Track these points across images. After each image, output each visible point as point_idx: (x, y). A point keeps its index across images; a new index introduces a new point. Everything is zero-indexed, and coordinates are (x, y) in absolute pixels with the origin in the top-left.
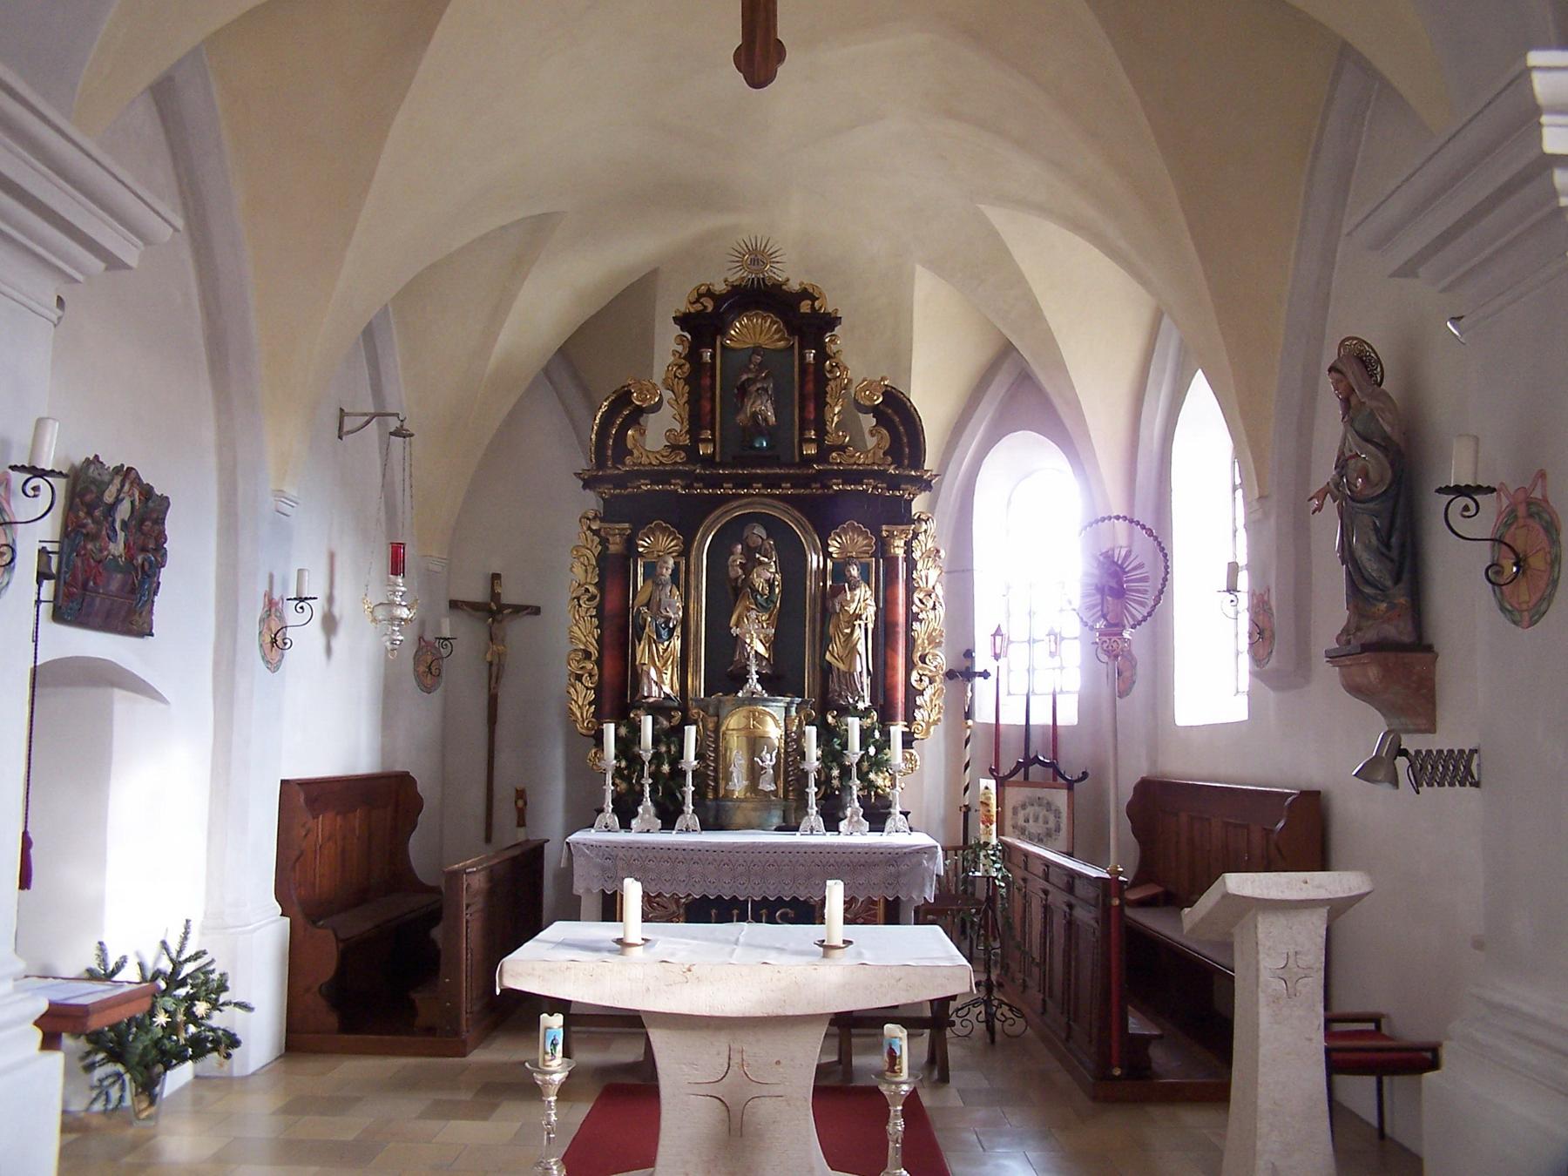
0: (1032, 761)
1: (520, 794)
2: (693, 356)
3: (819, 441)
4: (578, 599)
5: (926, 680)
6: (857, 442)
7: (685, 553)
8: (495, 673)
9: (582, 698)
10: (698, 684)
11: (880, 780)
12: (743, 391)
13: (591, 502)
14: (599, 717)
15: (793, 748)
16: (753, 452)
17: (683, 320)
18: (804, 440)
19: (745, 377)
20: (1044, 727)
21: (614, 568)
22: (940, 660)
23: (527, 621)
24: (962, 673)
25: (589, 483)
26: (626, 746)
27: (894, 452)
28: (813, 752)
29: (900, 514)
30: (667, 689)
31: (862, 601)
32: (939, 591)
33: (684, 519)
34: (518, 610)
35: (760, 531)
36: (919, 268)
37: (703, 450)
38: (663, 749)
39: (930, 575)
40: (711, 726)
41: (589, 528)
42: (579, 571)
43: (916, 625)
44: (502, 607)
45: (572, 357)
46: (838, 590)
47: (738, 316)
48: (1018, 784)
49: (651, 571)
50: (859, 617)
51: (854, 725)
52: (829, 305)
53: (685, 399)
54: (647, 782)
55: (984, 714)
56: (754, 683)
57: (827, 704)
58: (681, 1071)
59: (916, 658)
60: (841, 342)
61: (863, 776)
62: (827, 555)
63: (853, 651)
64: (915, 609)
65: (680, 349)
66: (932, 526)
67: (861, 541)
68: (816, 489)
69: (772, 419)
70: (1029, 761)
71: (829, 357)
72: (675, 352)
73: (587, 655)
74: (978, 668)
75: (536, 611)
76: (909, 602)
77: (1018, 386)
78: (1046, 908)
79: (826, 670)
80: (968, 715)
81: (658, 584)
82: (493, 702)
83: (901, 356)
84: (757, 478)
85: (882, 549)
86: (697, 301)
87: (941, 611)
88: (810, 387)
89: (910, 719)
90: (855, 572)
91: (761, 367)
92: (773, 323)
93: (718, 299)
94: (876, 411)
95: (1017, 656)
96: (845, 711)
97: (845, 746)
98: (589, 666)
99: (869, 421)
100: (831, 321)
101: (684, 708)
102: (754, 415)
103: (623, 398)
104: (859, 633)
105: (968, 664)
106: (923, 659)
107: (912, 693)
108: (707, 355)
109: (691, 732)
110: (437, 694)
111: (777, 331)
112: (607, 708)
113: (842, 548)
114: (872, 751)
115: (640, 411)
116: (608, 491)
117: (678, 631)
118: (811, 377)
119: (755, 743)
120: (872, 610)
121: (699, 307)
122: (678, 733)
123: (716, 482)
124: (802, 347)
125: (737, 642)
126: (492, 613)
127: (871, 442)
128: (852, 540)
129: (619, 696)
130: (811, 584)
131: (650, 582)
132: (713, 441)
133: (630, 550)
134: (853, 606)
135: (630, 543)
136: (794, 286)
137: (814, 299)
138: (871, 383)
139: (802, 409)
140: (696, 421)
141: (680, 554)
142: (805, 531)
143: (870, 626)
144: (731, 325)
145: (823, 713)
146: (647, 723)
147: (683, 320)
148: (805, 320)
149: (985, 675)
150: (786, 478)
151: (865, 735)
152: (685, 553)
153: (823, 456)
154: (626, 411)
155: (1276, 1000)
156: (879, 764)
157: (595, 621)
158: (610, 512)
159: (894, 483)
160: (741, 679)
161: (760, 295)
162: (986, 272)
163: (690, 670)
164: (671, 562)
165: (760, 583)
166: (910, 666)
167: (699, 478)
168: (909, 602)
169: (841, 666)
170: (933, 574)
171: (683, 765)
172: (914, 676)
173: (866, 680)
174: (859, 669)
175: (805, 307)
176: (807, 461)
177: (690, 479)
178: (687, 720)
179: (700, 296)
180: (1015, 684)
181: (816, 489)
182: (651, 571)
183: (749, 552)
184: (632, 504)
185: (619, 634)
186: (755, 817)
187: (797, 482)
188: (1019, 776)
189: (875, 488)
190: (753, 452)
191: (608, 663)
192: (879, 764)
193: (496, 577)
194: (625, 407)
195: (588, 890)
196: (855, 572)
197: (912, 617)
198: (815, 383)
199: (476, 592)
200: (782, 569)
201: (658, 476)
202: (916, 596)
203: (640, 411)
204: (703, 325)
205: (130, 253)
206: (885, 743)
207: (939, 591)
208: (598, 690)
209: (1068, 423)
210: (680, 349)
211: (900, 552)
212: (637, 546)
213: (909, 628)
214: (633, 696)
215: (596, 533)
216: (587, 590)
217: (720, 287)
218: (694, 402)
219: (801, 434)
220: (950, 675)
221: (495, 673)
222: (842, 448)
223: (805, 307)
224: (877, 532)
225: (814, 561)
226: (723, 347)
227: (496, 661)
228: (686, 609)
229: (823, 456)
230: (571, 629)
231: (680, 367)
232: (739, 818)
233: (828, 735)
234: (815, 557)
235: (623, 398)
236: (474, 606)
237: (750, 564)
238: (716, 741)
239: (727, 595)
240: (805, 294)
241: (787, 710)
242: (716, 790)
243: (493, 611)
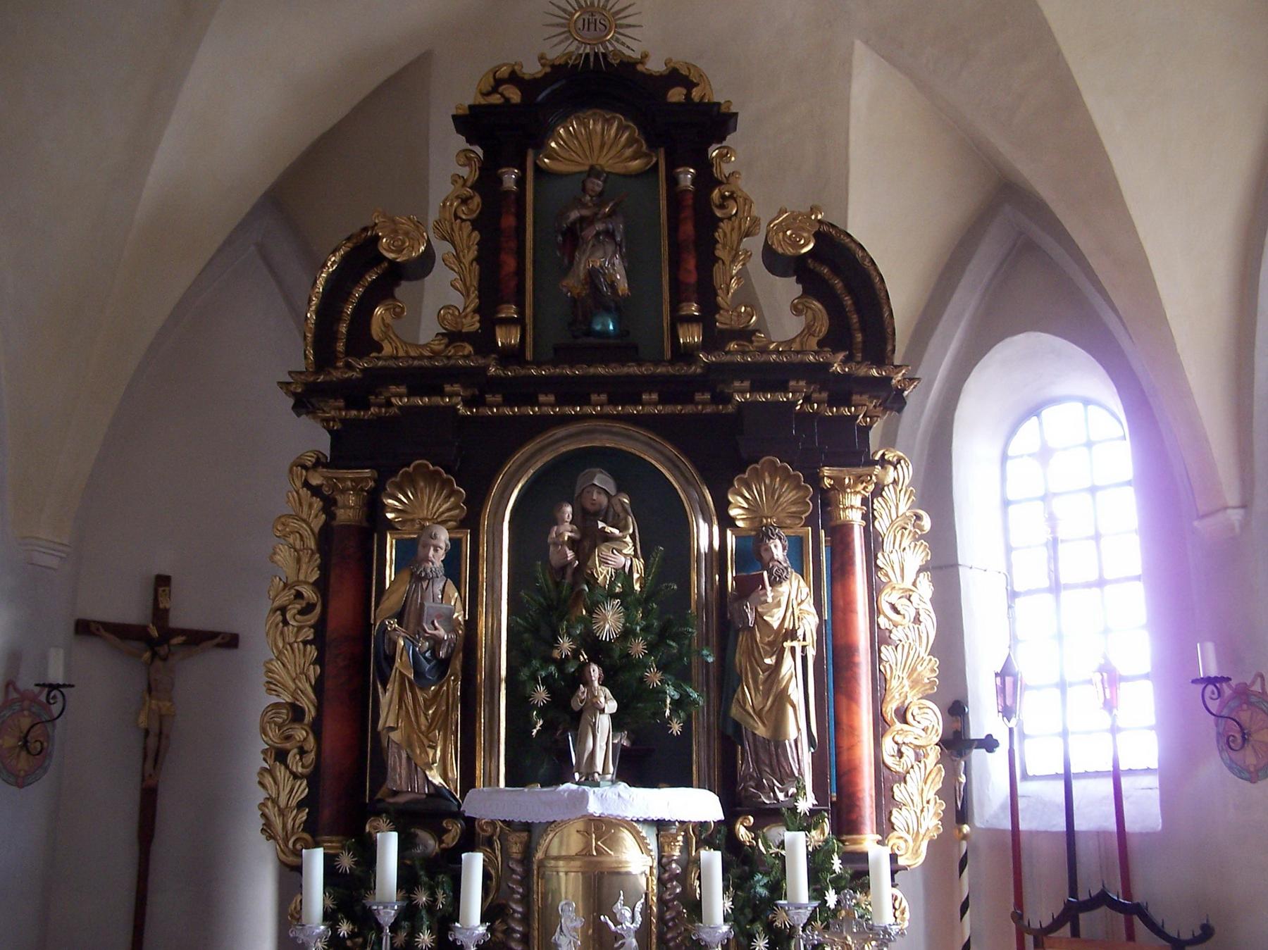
2: (487, 182)
4: (283, 610)
5: (909, 753)
7: (470, 521)
8: (155, 748)
12: (572, 238)
13: (314, 437)
16: (591, 340)
17: (472, 123)
18: (679, 319)
19: (574, 215)
20: (1100, 834)
21: (348, 551)
23: (213, 658)
25: (306, 399)
27: (836, 339)
28: (718, 904)
31: (791, 602)
34: (198, 639)
35: (602, 480)
36: (860, 48)
37: (506, 337)
38: (423, 898)
40: (516, 850)
41: (306, 484)
42: (284, 556)
43: (886, 652)
44: (168, 633)
45: (285, 201)
46: (750, 587)
47: (564, 119)
49: (410, 555)
50: (792, 635)
51: (798, 846)
52: (719, 90)
53: (473, 253)
59: (890, 709)
60: (737, 157)
62: (726, 522)
63: (782, 698)
64: (883, 622)
65: (465, 172)
67: (789, 495)
68: (702, 404)
69: (623, 285)
71: (719, 183)
72: (456, 178)
73: (297, 713)
74: (976, 733)
75: (232, 641)
82: (149, 798)
84: (600, 384)
85: (827, 501)
86: (494, 90)
88: (688, 229)
90: (778, 550)
91: (601, 198)
92: (621, 129)
95: (1036, 710)
96: (770, 816)
97: (777, 888)
98: (300, 734)
102: (593, 275)
103: (364, 252)
105: (958, 725)
106: (902, 715)
107: (885, 780)
108: (510, 178)
109: (474, 864)
110: (38, 791)
111: (629, 143)
112: (326, 814)
113: (753, 510)
116: (335, 409)
117: (457, 664)
118: (688, 213)
120: (809, 623)
123: (523, 392)
124: (672, 166)
126: (152, 644)
128: (771, 491)
130: (699, 584)
131: (406, 576)
132: (520, 322)
133: (374, 522)
134: (779, 613)
135: (374, 507)
136: (655, 65)
138: (794, 217)
139: (675, 264)
140: (492, 289)
141: (463, 524)
142: (687, 482)
143: (811, 653)
144: (549, 132)
146: (389, 846)
147: (472, 123)
148: (681, 122)
149: (989, 744)
150: (651, 382)
152: (470, 521)
154: (372, 272)
157: (312, 652)
158: (346, 449)
159: (841, 390)
161: (600, 82)
163: (481, 740)
164: (443, 536)
167: (495, 384)
168: (874, 611)
169: (761, 731)
172: (888, 746)
174: (792, 733)
176: (685, 354)
177: (479, 385)
178: (470, 842)
179: (498, 82)
180: (1042, 758)
181: (702, 404)
183: (585, 518)
187: (675, 390)
189: (807, 400)
190: (591, 340)
191: (331, 728)
193: (163, 581)
194: (368, 267)
196: (778, 550)
197: (879, 638)
198: (697, 225)
199: (129, 608)
200: (645, 551)
201: (425, 379)
202: (885, 600)
203: (396, 273)
208: (313, 779)
210: (465, 172)
211: (855, 517)
212: (384, 508)
214: (374, 791)
215: (316, 491)
216: (299, 595)
217: (532, 69)
218: (488, 259)
219: (674, 309)
221: (155, 748)
223: (676, 95)
225: (704, 535)
226: (540, 171)
227: (155, 727)
230: (274, 670)
231: (465, 201)
234: (704, 527)
235: (364, 252)
236: (122, 632)
237: (589, 540)
238: (526, 880)
240: (675, 77)
243: (157, 641)
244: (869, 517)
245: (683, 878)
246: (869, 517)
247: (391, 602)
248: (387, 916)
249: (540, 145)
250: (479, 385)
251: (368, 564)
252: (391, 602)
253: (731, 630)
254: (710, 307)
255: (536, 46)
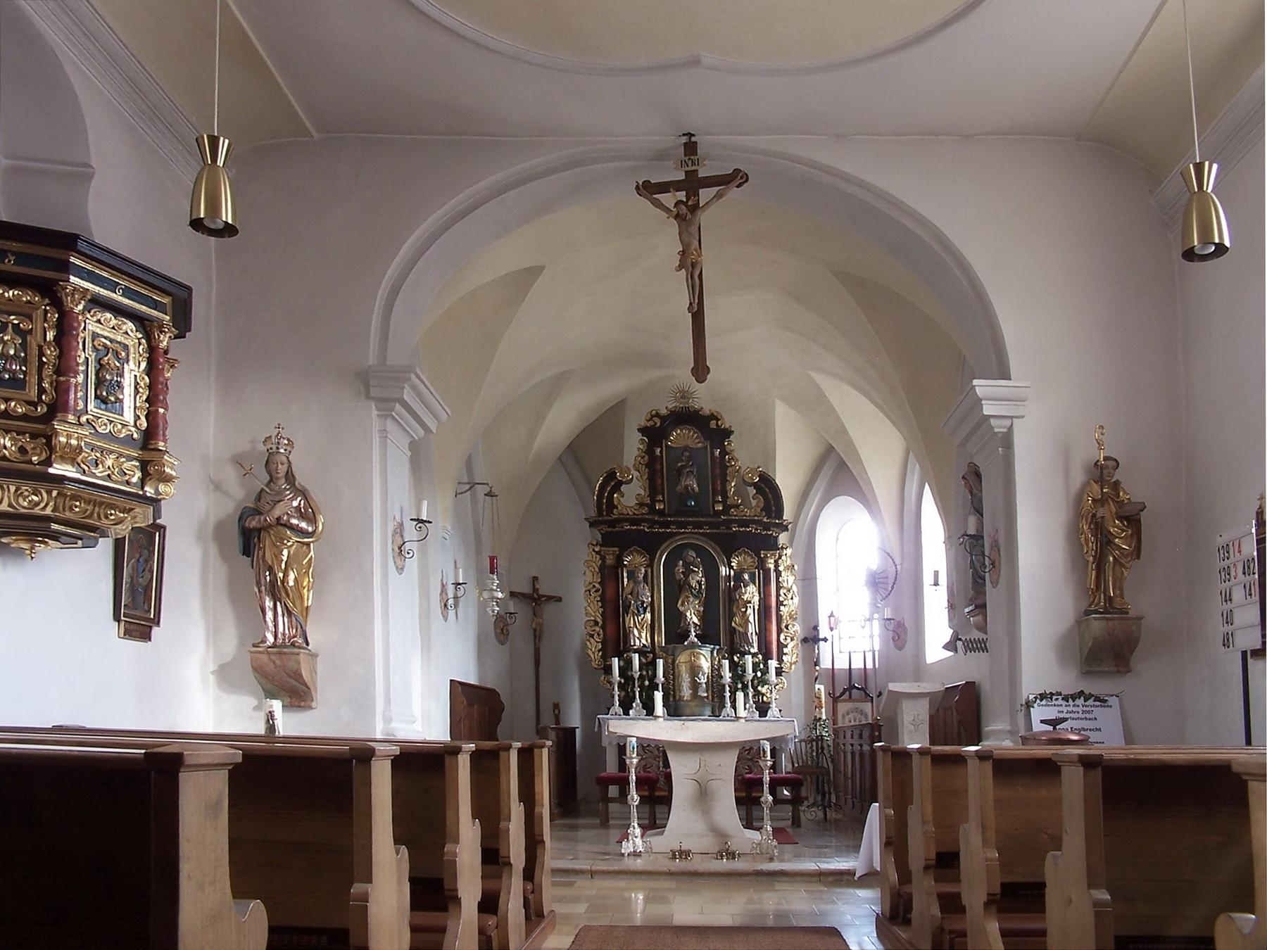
0: (852, 687)
1: (556, 706)
2: (649, 451)
3: (724, 502)
6: (746, 503)
9: (594, 647)
10: (661, 639)
11: (764, 690)
12: (679, 472)
14: (606, 657)
15: (716, 672)
21: (610, 574)
22: (797, 629)
24: (811, 639)
26: (626, 669)
27: (767, 509)
28: (727, 675)
29: (773, 545)
30: (644, 641)
31: (751, 593)
32: (795, 588)
33: (650, 546)
34: (550, 598)
39: (788, 579)
44: (541, 597)
46: (737, 587)
47: (674, 429)
48: (845, 701)
54: (637, 690)
55: (826, 663)
56: (693, 637)
57: (733, 647)
58: (682, 770)
61: (755, 688)
63: (747, 621)
66: (789, 551)
67: (749, 560)
69: (697, 489)
70: (852, 687)
73: (596, 623)
74: (821, 636)
75: (559, 599)
76: (778, 595)
77: (837, 471)
78: (853, 753)
79: (733, 632)
80: (816, 664)
81: (636, 582)
83: (769, 455)
85: (762, 564)
87: (796, 600)
88: (718, 471)
89: (780, 660)
90: (746, 577)
93: (663, 418)
94: (755, 485)
95: (844, 628)
96: (743, 654)
98: (597, 629)
99: (752, 491)
100: (727, 433)
101: (653, 651)
102: (687, 487)
103: (611, 475)
104: (750, 611)
106: (787, 627)
107: (781, 646)
109: (660, 663)
114: (759, 674)
115: (620, 483)
116: (606, 529)
119: (695, 670)
120: (756, 599)
121: (651, 423)
122: (653, 664)
125: (682, 615)
126: (534, 600)
127: (754, 503)
129: (617, 644)
130: (722, 584)
132: (663, 501)
135: (619, 559)
136: (706, 411)
137: (718, 420)
140: (653, 490)
142: (718, 554)
145: (732, 654)
147: (643, 430)
148: (714, 432)
149: (825, 640)
151: (755, 666)
152: (650, 565)
153: (726, 511)
154: (613, 482)
155: (910, 732)
156: (764, 682)
158: (607, 541)
159: (767, 527)
160: (686, 635)
161: (687, 417)
162: (814, 406)
165: (694, 584)
166: (779, 631)
168: (778, 595)
170: (791, 579)
171: (657, 681)
172: (782, 637)
173: (755, 638)
175: (713, 424)
176: (718, 513)
177: (652, 523)
181: (723, 530)
182: (632, 575)
183: (686, 565)
184: (617, 536)
185: (614, 610)
186: (696, 710)
187: (713, 525)
188: (847, 695)
192: (764, 682)
193: (535, 579)
195: (610, 743)
196: (746, 577)
198: (722, 468)
199: (525, 588)
200: (705, 575)
201: (635, 521)
202: (782, 592)
204: (654, 434)
205: (432, 425)
206: (765, 672)
207: (795, 588)
209: (868, 496)
211: (772, 566)
213: (778, 610)
217: (664, 412)
218: (652, 478)
220: (805, 640)
221: (537, 635)
222: (737, 506)
224: (758, 555)
225: (724, 571)
226: (667, 446)
228: (652, 597)
229: (726, 511)
232: (688, 711)
233: (734, 666)
235: (611, 475)
236: (524, 595)
239: (676, 589)
240: (713, 417)
241: (712, 652)
242: (674, 696)
244: (777, 566)
245: (718, 670)
246: (777, 566)
247: (628, 590)
248: (637, 676)
249: (667, 438)
250: (652, 523)
251: (617, 579)
252: (628, 590)
253: (733, 600)
254: (725, 497)
255: (665, 405)
